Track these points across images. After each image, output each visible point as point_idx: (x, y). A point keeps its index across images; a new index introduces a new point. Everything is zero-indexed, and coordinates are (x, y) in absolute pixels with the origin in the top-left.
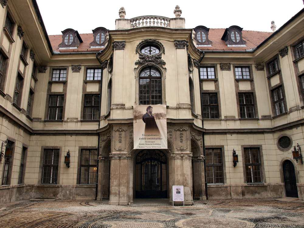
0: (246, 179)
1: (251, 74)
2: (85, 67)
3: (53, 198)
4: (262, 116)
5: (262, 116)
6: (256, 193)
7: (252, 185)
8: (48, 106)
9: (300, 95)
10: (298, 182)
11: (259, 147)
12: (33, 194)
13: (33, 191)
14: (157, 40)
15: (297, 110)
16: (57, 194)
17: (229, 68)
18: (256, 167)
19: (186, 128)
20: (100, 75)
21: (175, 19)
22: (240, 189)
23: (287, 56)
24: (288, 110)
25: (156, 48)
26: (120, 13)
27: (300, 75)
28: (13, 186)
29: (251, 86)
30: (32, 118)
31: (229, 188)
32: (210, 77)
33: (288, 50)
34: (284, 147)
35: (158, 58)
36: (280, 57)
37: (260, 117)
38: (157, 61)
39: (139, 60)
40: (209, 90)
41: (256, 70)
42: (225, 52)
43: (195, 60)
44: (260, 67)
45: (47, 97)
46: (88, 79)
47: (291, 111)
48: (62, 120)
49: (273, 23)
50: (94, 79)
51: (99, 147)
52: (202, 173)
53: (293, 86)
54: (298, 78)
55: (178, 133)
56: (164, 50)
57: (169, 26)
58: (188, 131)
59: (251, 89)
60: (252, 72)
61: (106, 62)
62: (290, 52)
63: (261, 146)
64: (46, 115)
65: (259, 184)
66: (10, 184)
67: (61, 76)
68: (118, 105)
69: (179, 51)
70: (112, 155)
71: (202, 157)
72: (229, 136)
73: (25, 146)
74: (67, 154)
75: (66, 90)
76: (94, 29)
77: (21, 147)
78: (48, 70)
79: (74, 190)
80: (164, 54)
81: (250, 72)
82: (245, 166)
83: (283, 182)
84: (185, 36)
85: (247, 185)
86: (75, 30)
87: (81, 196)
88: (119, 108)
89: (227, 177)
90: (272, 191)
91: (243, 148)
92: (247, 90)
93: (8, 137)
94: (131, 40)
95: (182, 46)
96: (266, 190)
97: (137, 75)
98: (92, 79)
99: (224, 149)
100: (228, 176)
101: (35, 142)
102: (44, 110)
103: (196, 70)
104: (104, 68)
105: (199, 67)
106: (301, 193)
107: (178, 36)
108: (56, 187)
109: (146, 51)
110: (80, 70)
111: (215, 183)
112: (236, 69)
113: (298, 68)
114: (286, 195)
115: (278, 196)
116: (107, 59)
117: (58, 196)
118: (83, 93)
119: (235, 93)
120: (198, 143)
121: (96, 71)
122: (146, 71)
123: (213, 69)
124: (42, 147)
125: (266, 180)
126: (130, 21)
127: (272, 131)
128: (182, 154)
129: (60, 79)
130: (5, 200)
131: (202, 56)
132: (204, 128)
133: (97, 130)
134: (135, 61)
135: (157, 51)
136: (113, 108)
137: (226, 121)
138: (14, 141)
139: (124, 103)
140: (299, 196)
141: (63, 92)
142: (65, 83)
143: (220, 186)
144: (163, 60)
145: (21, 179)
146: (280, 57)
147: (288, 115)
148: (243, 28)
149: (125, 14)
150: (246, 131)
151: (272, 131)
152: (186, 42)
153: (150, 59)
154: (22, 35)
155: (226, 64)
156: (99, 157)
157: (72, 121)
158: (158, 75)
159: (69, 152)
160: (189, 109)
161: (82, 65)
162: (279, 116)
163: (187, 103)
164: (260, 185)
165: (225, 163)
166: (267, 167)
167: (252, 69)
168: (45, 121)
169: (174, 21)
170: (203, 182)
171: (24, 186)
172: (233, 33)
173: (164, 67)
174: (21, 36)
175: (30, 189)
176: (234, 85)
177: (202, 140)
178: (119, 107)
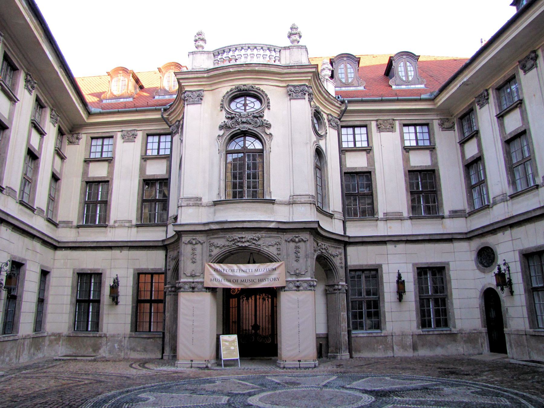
0: (420, 322)
1: (432, 136)
2: (143, 133)
4: (450, 211)
5: (450, 211)
6: (437, 346)
7: (431, 333)
8: (83, 201)
9: (507, 174)
10: (506, 327)
11: (443, 265)
12: (60, 348)
14: (257, 86)
15: (503, 200)
16: (99, 348)
17: (392, 127)
18: (423, 301)
19: (305, 236)
20: (168, 145)
21: (288, 48)
22: (408, 340)
23: (487, 105)
24: (491, 201)
25: (256, 100)
26: (196, 41)
27: (507, 139)
28: (24, 336)
30: (57, 223)
31: (389, 338)
32: (358, 145)
33: (488, 95)
34: (486, 264)
36: (478, 107)
37: (446, 213)
38: (256, 123)
39: (226, 121)
40: (356, 168)
41: (441, 129)
43: (331, 115)
44: (447, 125)
45: (82, 185)
46: (149, 153)
47: (495, 203)
48: (107, 223)
49: (482, 39)
50: (158, 152)
51: (166, 269)
52: (342, 313)
53: (497, 158)
54: (504, 145)
55: (292, 245)
56: (269, 103)
57: (279, 61)
58: (309, 242)
60: (434, 134)
61: (177, 123)
62: (492, 99)
64: (81, 217)
66: (18, 332)
67: (105, 148)
68: (190, 199)
69: (296, 103)
70: (180, 284)
71: (343, 285)
73: (45, 269)
74: (114, 282)
75: (528, 123)
77: (39, 271)
78: (84, 138)
79: (126, 343)
80: (269, 109)
81: (430, 133)
82: (418, 299)
83: (485, 327)
84: (306, 77)
85: (422, 333)
88: (191, 205)
89: (387, 320)
90: (465, 342)
91: (416, 268)
92: (425, 165)
93: (12, 255)
95: (300, 94)
96: (455, 341)
97: (223, 148)
98: (155, 153)
99: (382, 271)
101: (62, 261)
102: (77, 207)
103: (332, 134)
104: (175, 133)
105: (339, 127)
106: (511, 345)
107: (293, 77)
108: (97, 337)
109: (239, 105)
110: (135, 138)
111: (366, 330)
112: (405, 129)
113: (504, 128)
114: (489, 349)
115: (476, 352)
116: (179, 119)
117: (101, 351)
118: (140, 177)
120: (335, 261)
121: (163, 138)
122: (237, 140)
123: (364, 130)
124: (74, 270)
125: (456, 323)
126: (212, 55)
127: (468, 237)
128: (298, 281)
129: (104, 153)
130: (8, 359)
131: (343, 108)
132: (348, 234)
133: (163, 241)
134: (220, 123)
135: (257, 105)
136: (182, 205)
137: (386, 220)
138: (23, 262)
139: (199, 196)
140: (508, 351)
141: (107, 177)
142: (110, 161)
143: (375, 335)
144: (267, 119)
145: (39, 324)
146: (478, 107)
147: (491, 209)
148: (419, 56)
149: (205, 43)
151: (468, 237)
152: (306, 88)
153: (244, 120)
155: (387, 120)
156: (167, 286)
157: (121, 225)
158: (258, 145)
159: (117, 279)
160: (310, 203)
162: (479, 210)
163: (307, 193)
164: (445, 332)
165: (383, 295)
166: (458, 300)
167: (433, 129)
168: (78, 227)
169: (288, 52)
170: (344, 328)
171: (46, 334)
172: (402, 64)
174: (31, 89)
175: (56, 340)
177: (343, 254)
178: (191, 203)
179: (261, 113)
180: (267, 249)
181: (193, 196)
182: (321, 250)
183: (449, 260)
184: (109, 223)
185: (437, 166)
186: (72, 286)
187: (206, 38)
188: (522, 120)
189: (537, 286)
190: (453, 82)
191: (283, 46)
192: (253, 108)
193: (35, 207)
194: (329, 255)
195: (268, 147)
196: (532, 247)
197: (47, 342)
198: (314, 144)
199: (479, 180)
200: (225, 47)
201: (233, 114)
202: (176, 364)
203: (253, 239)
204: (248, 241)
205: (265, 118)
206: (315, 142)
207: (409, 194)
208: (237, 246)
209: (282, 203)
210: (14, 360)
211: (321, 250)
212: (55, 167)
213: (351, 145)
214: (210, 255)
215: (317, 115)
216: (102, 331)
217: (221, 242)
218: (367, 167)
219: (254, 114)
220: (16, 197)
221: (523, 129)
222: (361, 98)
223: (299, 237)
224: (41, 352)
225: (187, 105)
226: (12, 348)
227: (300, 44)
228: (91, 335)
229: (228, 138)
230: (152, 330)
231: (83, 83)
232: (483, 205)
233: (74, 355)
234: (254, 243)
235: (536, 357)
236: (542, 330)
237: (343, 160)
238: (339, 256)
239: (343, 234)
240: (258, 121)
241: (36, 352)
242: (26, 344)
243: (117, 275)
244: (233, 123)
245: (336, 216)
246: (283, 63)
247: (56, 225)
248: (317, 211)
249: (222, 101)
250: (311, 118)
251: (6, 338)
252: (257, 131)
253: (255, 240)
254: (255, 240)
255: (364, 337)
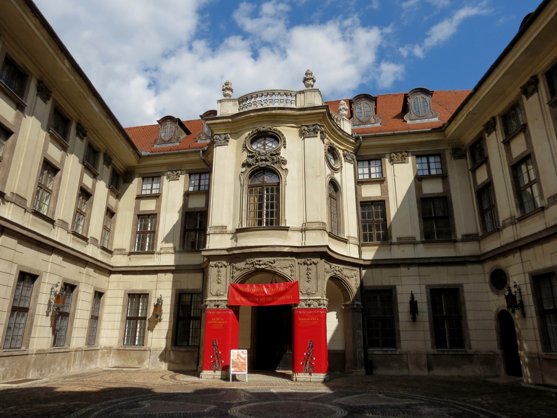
3: (138, 366)
7: (446, 353)
8: (135, 231)
9: (515, 198)
12: (111, 360)
13: (111, 355)
16: (143, 361)
20: (207, 181)
21: (303, 92)
24: (501, 225)
25: (274, 140)
26: (223, 90)
27: (513, 164)
29: (443, 187)
30: (113, 250)
31: (404, 357)
35: (275, 155)
36: (486, 135)
37: (459, 237)
38: (273, 160)
40: (371, 197)
41: (452, 158)
42: (377, 135)
45: (134, 217)
47: (504, 227)
56: (285, 142)
59: (444, 192)
62: (499, 126)
63: (461, 285)
64: (133, 245)
65: (457, 351)
69: (309, 141)
70: (206, 303)
71: (358, 305)
72: (403, 270)
75: (532, 147)
76: (202, 114)
77: (92, 291)
80: (285, 147)
85: (436, 353)
86: (176, 117)
87: (177, 365)
92: (436, 192)
94: (238, 131)
99: (396, 292)
100: (403, 335)
102: (130, 236)
109: (259, 146)
117: (145, 363)
119: (416, 199)
124: (125, 291)
129: (153, 190)
130: (58, 368)
134: (243, 161)
137: (399, 245)
138: (76, 284)
139: (224, 225)
142: (157, 197)
143: (390, 353)
146: (486, 135)
150: (432, 261)
152: (318, 127)
153: (263, 158)
154: (85, 135)
159: (161, 298)
161: (182, 169)
164: (460, 353)
167: (445, 158)
168: (130, 254)
169: (302, 95)
171: (99, 348)
173: (284, 167)
176: (414, 187)
179: (278, 151)
180: (281, 271)
181: (220, 225)
182: (335, 272)
183: (463, 282)
184: (156, 250)
185: (450, 194)
186: (123, 305)
187: (232, 87)
188: (526, 145)
189: (548, 308)
190: (460, 113)
191: (298, 90)
192: (271, 146)
193: (88, 237)
194: (344, 277)
195: (283, 180)
196: (541, 269)
197: (100, 355)
198: (327, 176)
199: (490, 205)
200: (248, 94)
201: (253, 153)
202: (201, 375)
203: (270, 262)
204: (265, 264)
205: (281, 155)
206: (329, 175)
207: (422, 219)
208: (255, 268)
209: (294, 230)
210: (65, 369)
211: (335, 272)
212: (109, 203)
213: (367, 177)
214: (233, 277)
215: (332, 151)
216: (147, 345)
217: (241, 265)
218: (381, 197)
219: (271, 152)
220: (67, 228)
221: (527, 153)
222: (374, 134)
223: (311, 260)
224: (93, 364)
225: (216, 146)
226: (63, 359)
227: (314, 88)
228: (137, 349)
229: (249, 173)
230: (190, 344)
231: (143, 131)
232: (494, 228)
233: (122, 366)
234: (270, 266)
235: (549, 381)
236: (556, 354)
237: (358, 191)
238: (354, 277)
239: (358, 257)
240: (275, 158)
241: (88, 363)
242: (77, 356)
243: (161, 295)
244: (253, 161)
245: (351, 240)
246: (299, 106)
247: (110, 252)
248: (329, 236)
249: (245, 142)
250: (323, 154)
251: (57, 350)
252: (274, 167)
253: (272, 263)
254: (272, 263)
255: (380, 354)
